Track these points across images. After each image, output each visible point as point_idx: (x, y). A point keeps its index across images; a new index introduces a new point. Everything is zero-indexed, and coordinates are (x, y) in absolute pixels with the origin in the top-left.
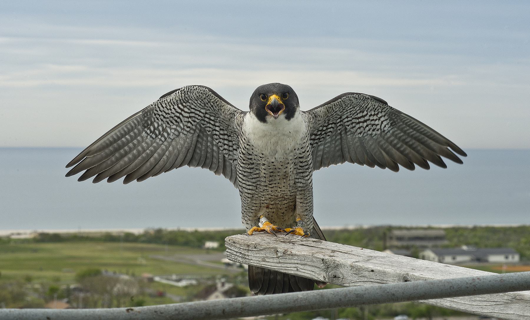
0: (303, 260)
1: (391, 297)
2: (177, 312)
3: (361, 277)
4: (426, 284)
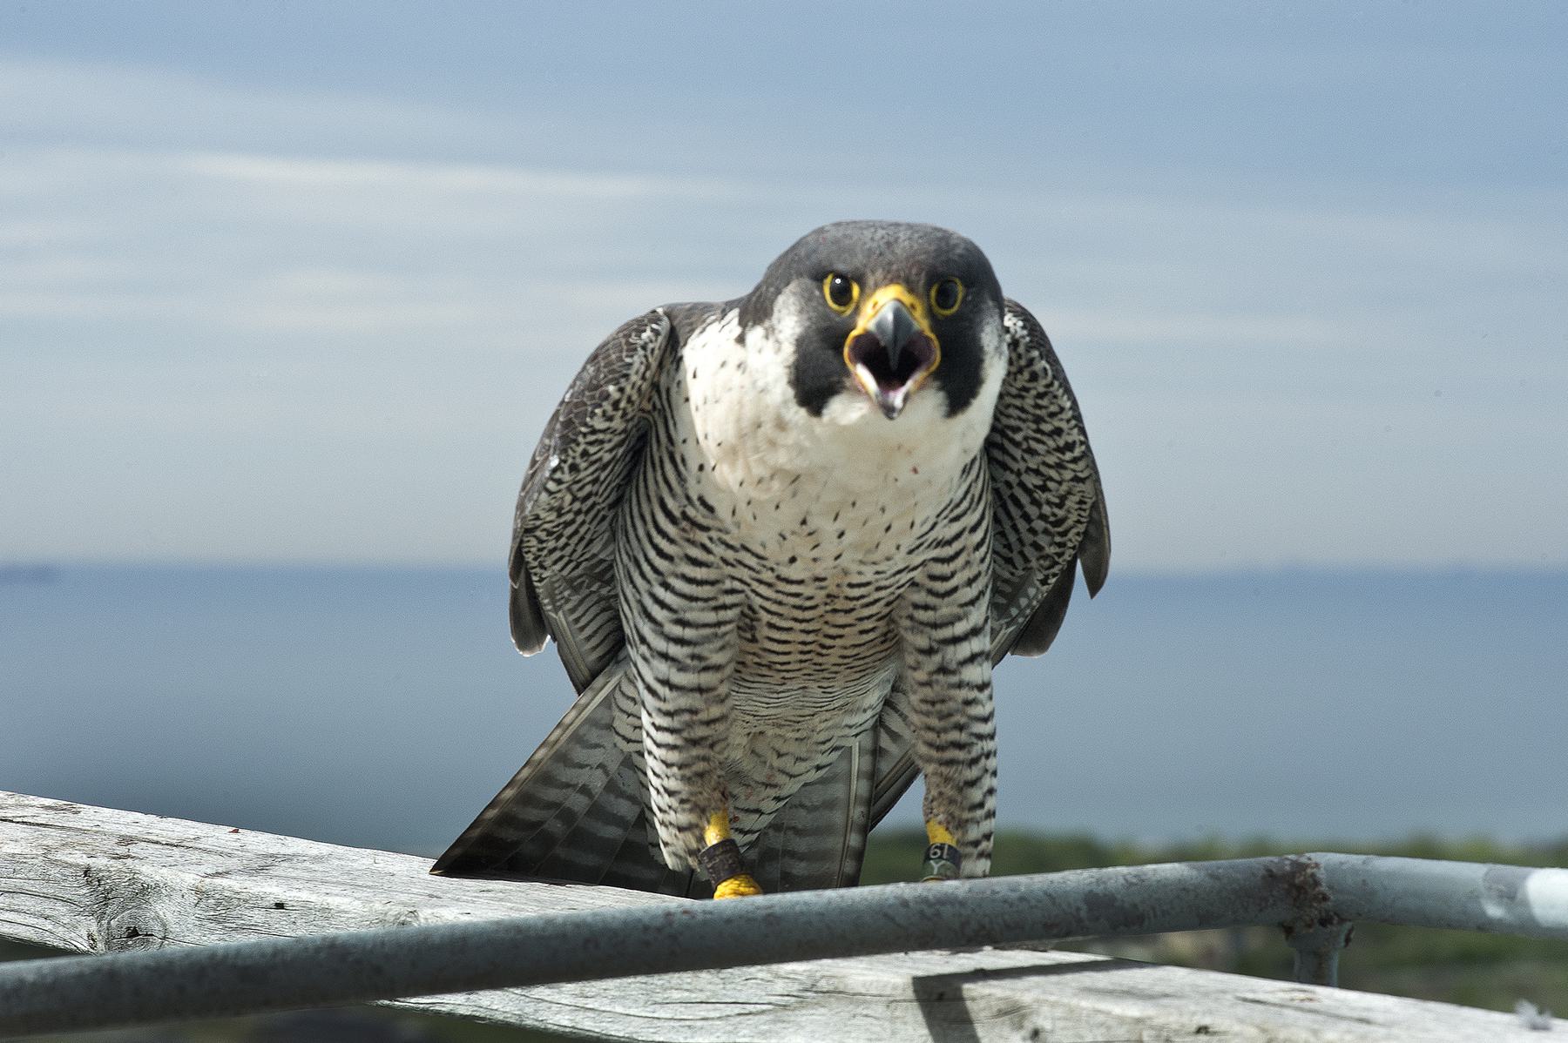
3: (235, 929)
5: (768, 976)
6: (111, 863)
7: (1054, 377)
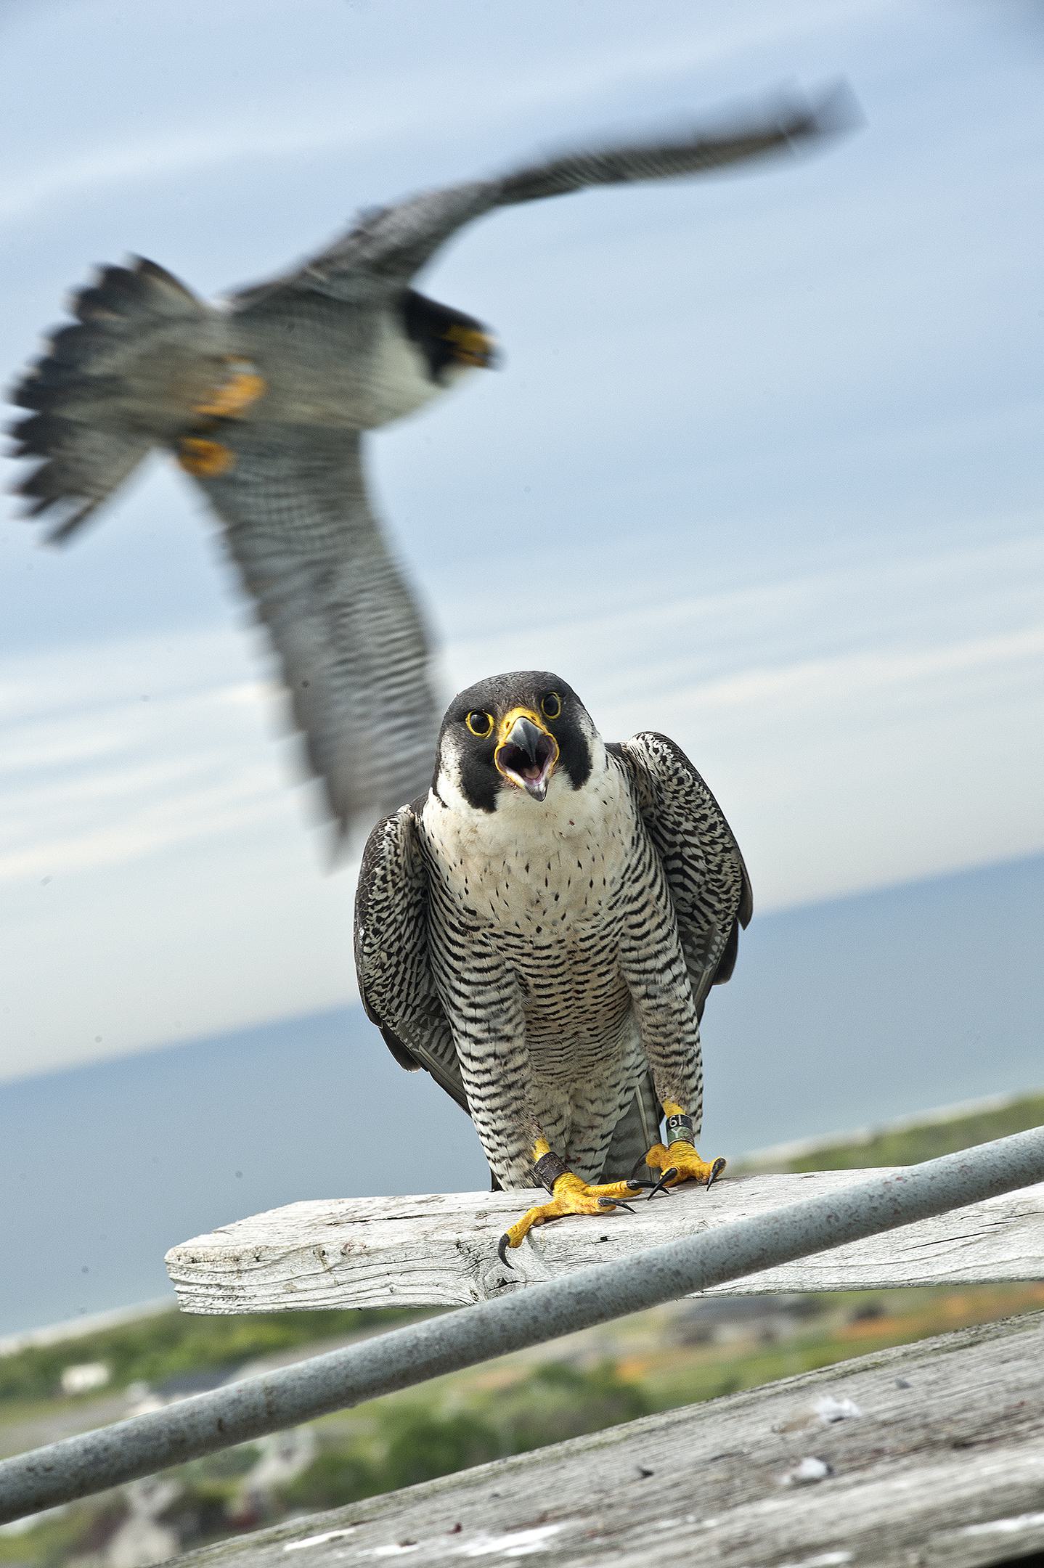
0: (404, 1261)
1: (673, 1280)
2: (91, 1457)
3: (576, 1263)
4: (759, 1225)
5: (978, 1213)
6: (474, 1234)
7: (694, 779)
